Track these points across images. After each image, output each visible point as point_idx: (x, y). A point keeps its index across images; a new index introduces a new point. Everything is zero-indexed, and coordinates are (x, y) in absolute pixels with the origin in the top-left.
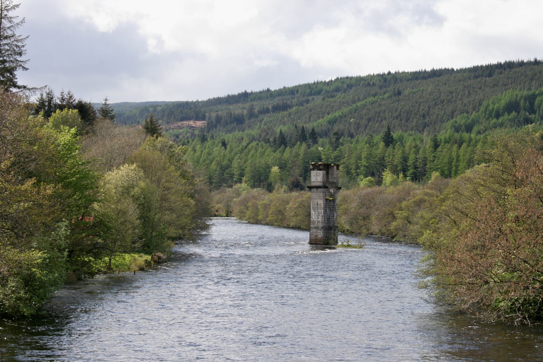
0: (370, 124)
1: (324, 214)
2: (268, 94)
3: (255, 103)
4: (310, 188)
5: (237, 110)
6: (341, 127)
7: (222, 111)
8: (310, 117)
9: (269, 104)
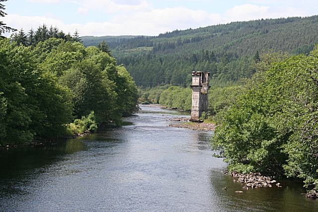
0: (249, 50)
1: (200, 102)
2: (190, 31)
3: (182, 37)
4: (192, 87)
5: (172, 40)
6: (231, 51)
7: (162, 41)
8: (214, 46)
9: (190, 37)
